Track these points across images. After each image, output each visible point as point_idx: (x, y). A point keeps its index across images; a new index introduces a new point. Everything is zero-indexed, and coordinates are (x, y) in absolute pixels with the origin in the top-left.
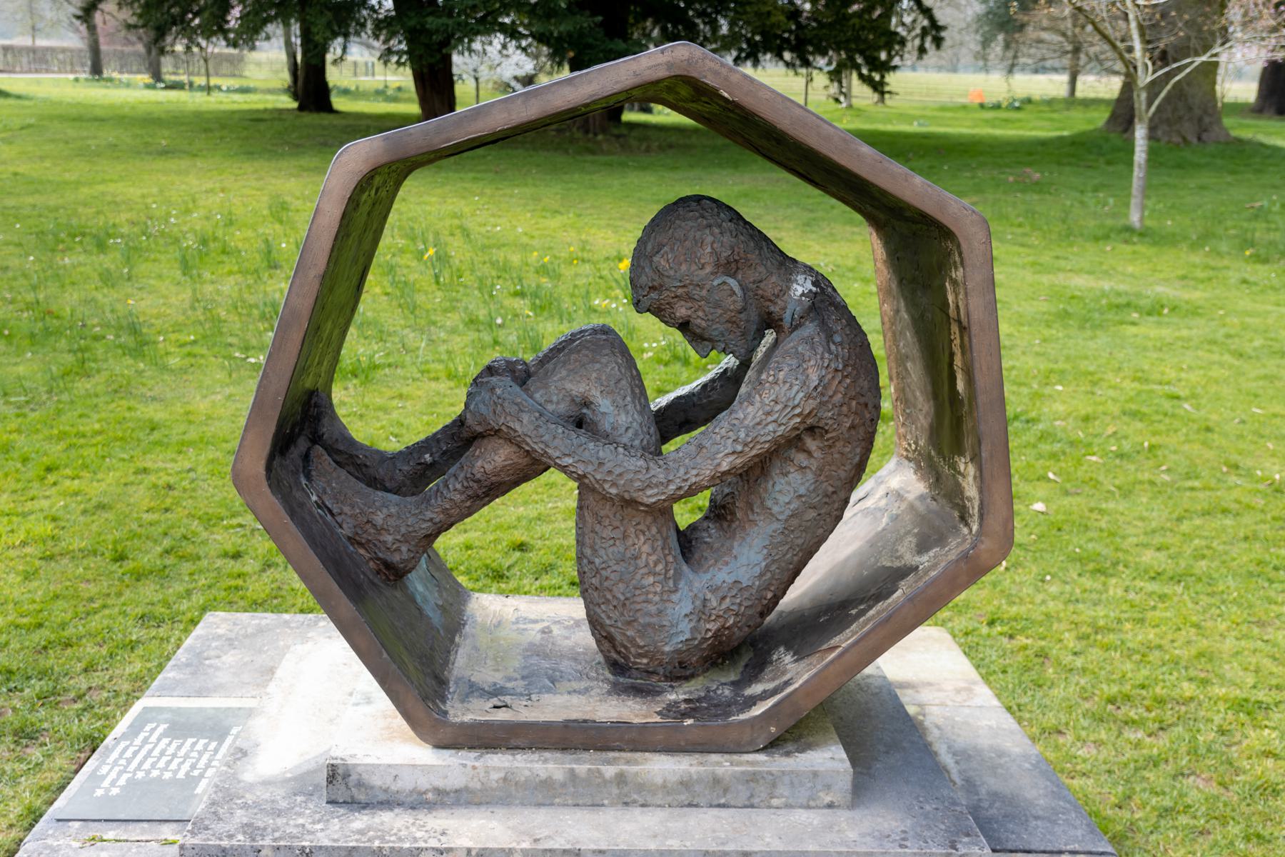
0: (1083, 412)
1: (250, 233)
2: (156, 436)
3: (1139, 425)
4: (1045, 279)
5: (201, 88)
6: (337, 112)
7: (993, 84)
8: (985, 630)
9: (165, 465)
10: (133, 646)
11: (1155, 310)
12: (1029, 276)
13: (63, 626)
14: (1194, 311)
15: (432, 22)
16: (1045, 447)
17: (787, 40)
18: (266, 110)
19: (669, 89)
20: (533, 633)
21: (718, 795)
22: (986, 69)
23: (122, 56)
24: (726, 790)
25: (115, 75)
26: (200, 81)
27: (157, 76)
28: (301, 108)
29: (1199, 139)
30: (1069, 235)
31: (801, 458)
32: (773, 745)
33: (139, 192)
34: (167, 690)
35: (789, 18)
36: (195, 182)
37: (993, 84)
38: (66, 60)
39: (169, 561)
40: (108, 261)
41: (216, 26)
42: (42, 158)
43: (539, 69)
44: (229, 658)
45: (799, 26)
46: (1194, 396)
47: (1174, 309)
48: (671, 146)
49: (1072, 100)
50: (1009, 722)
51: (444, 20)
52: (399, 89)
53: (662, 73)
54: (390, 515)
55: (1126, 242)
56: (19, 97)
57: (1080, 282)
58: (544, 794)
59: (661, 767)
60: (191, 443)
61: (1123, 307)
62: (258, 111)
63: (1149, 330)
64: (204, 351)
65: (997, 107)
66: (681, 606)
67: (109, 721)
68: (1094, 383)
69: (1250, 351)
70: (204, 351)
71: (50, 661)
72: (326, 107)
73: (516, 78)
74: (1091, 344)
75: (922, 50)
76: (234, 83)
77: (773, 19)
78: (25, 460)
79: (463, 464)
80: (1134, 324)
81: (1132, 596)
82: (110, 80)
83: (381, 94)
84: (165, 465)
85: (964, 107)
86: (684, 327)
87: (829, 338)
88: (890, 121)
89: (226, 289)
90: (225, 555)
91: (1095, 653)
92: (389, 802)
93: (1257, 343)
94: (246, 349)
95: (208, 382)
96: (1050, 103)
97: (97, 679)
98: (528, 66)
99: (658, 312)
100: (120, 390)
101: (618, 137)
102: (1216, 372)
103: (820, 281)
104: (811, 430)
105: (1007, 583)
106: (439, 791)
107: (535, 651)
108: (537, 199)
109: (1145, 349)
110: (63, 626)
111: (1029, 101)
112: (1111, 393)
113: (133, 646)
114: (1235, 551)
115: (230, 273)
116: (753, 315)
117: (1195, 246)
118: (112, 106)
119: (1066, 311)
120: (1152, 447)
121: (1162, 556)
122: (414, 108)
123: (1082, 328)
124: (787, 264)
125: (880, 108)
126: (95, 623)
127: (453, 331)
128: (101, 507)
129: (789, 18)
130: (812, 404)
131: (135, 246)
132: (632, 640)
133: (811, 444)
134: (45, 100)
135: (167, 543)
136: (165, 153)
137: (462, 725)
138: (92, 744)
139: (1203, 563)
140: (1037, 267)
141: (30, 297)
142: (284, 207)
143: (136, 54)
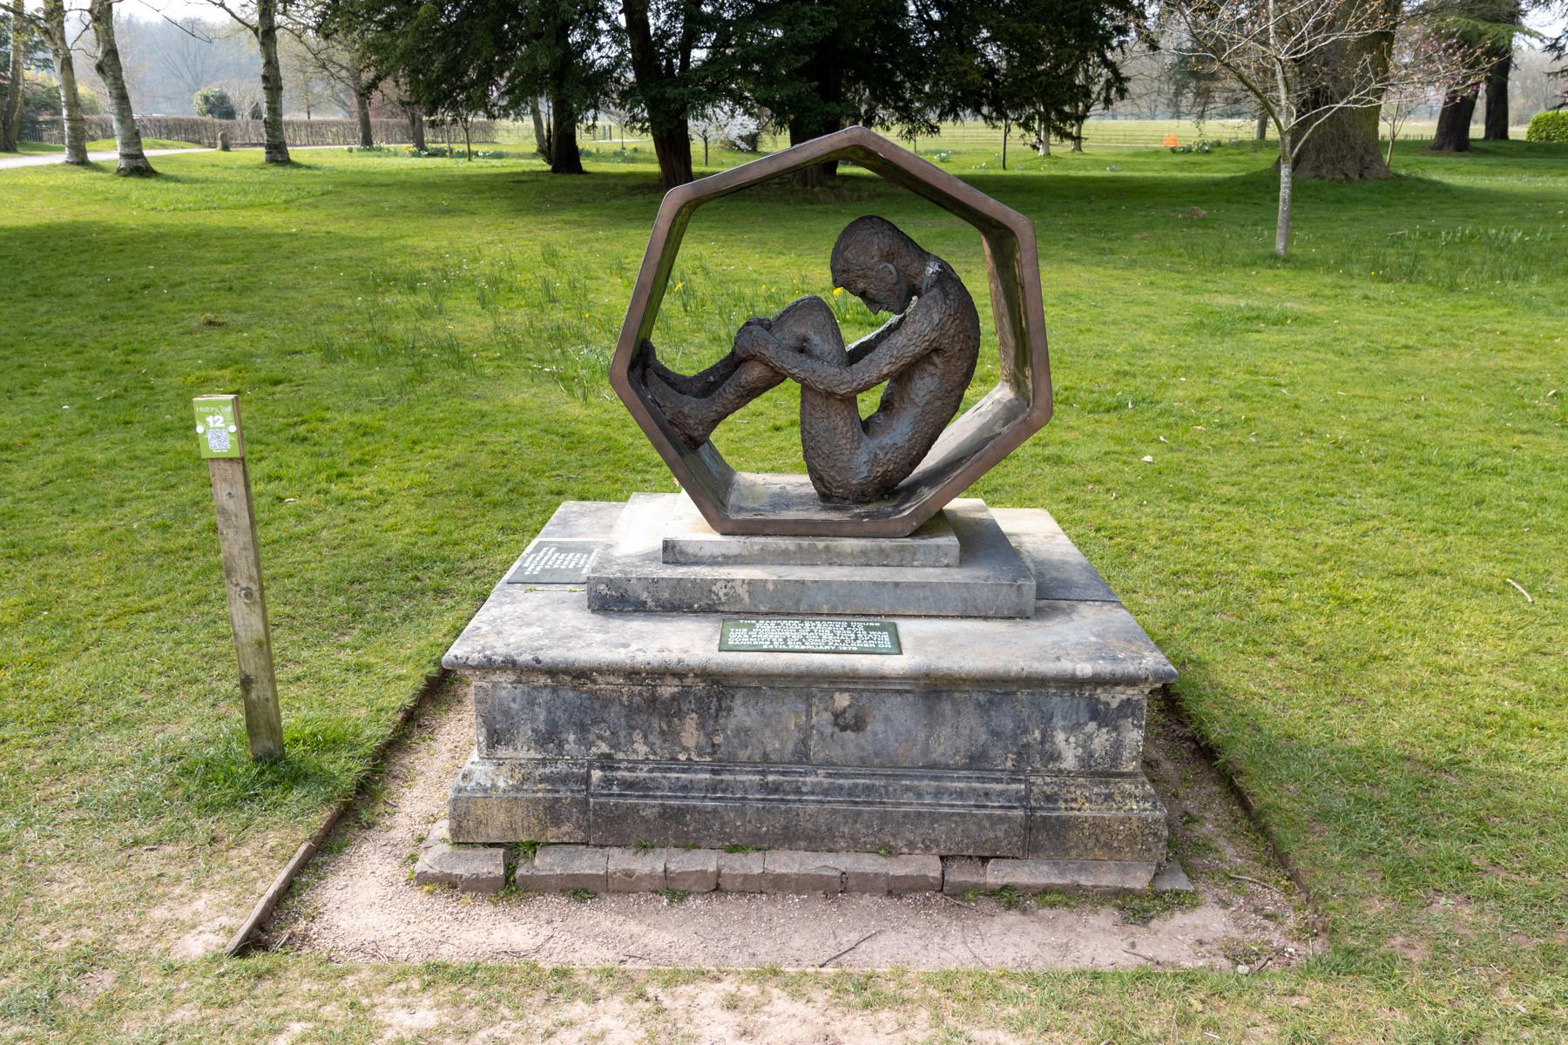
0: (1198, 396)
1: (529, 276)
2: (486, 421)
3: (1241, 404)
4: (1191, 299)
5: (461, 155)
6: (585, 173)
7: (1185, 130)
8: (1093, 534)
9: (498, 439)
10: (500, 545)
11: (1279, 321)
12: (1179, 297)
13: (451, 533)
14: (1312, 321)
15: (670, 92)
16: (1161, 421)
17: (986, 96)
18: (524, 173)
19: (853, 152)
20: (776, 488)
21: (883, 559)
22: (1177, 115)
23: (388, 127)
24: (887, 556)
25: (383, 145)
26: (463, 148)
27: (421, 145)
28: (554, 170)
29: (1361, 176)
30: (1220, 264)
31: (931, 369)
32: (915, 534)
33: (433, 244)
34: (547, 535)
35: (984, 77)
36: (476, 235)
37: (1185, 130)
38: (339, 134)
39: (514, 496)
40: (423, 299)
41: (481, 103)
42: (346, 219)
43: (761, 128)
44: (583, 521)
45: (996, 83)
46: (1292, 384)
47: (1296, 319)
48: (879, 195)
49: (1261, 142)
50: (1076, 550)
51: (681, 90)
52: (636, 150)
53: (845, 144)
54: (691, 406)
55: (1270, 267)
56: (309, 167)
57: (1223, 301)
58: (784, 558)
59: (849, 544)
60: (512, 425)
61: (1254, 319)
62: (517, 174)
63: (1272, 336)
64: (508, 364)
65: (1188, 151)
66: (862, 457)
67: (492, 585)
68: (1212, 375)
69: (1351, 351)
70: (508, 364)
71: (447, 551)
72: (578, 169)
73: (741, 137)
74: (1218, 347)
75: (1108, 102)
76: (489, 149)
77: (969, 78)
78: (396, 437)
79: (736, 377)
80: (1258, 331)
81: (1205, 513)
82: (380, 149)
83: (619, 155)
84: (498, 439)
85: (1157, 152)
86: (863, 295)
87: (946, 295)
88: (1085, 167)
89: (519, 319)
90: (552, 493)
91: (1170, 548)
92: (698, 561)
93: (1359, 345)
94: (542, 361)
95: (515, 385)
96: (1239, 145)
97: (479, 563)
98: (751, 125)
99: (848, 286)
100: (452, 392)
101: (833, 188)
102: (1318, 366)
103: (944, 266)
104: (936, 351)
105: (1115, 506)
106: (725, 557)
107: (774, 495)
108: (763, 243)
109: (1263, 350)
110: (451, 533)
111: (1218, 144)
112: (1226, 382)
113: (500, 545)
114: (1290, 486)
115: (519, 306)
116: (904, 286)
117: (1329, 270)
118: (388, 173)
119: (1201, 322)
120: (1246, 420)
121: (1234, 489)
122: (655, 168)
123: (1213, 335)
124: (924, 255)
125: (1077, 155)
126: (471, 532)
127: (701, 346)
128: (457, 465)
129: (984, 77)
130: (935, 334)
131: (445, 282)
132: (833, 478)
133: (937, 360)
134: (331, 169)
135: (510, 485)
136: (447, 212)
137: (737, 521)
138: (483, 598)
139: (1264, 494)
140: (1188, 289)
141: (369, 326)
142: (554, 254)
143: (398, 125)
